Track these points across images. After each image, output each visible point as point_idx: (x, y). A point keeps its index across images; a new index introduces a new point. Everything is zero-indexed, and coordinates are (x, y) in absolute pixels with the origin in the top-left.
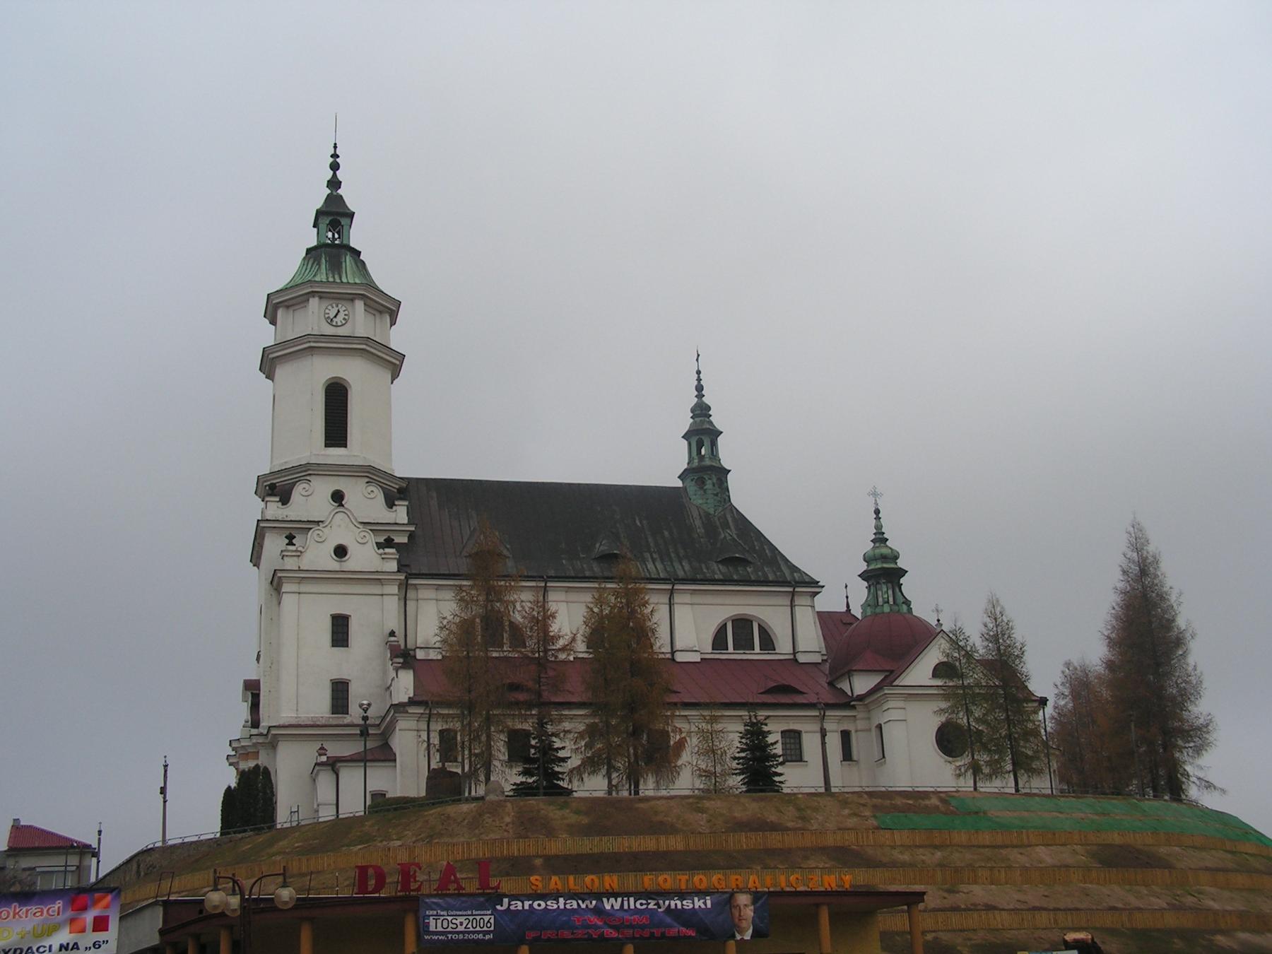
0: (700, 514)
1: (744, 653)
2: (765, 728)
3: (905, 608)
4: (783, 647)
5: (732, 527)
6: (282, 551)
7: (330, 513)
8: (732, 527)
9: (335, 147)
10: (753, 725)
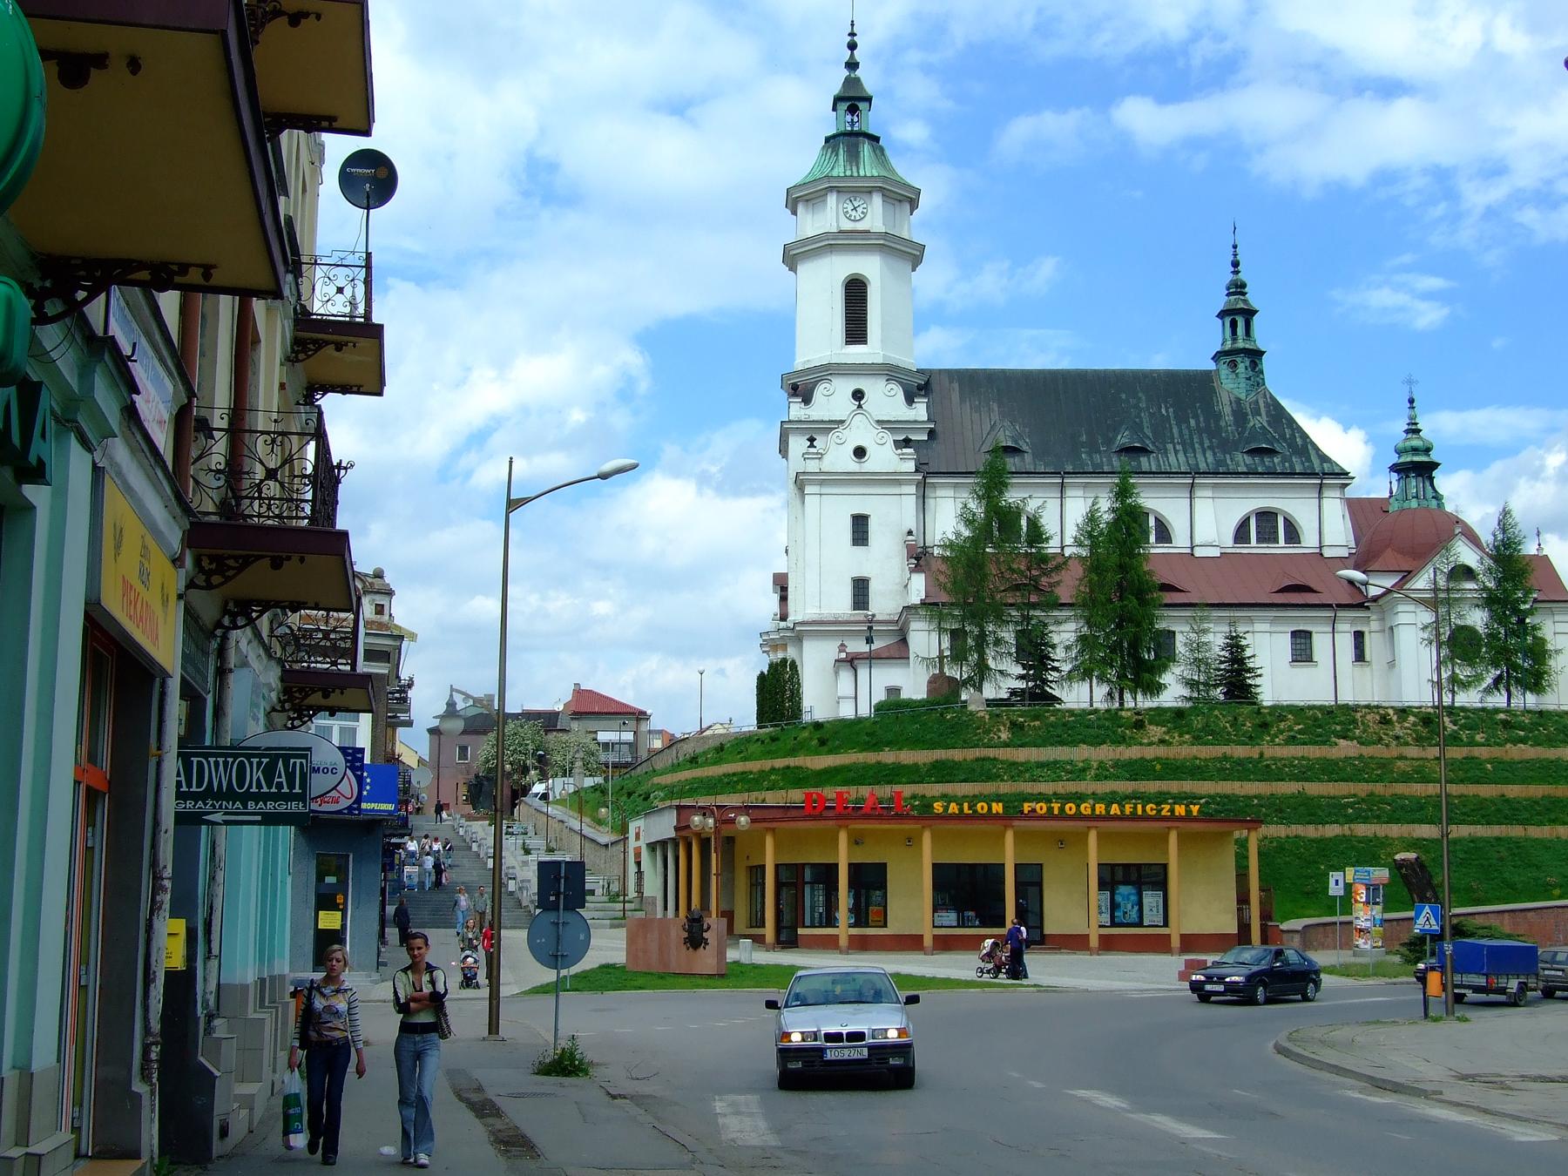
0: (1230, 401)
1: (1268, 547)
2: (1243, 642)
3: (1434, 502)
4: (1309, 540)
5: (1263, 413)
6: (803, 454)
7: (850, 414)
8: (1263, 413)
9: (852, 25)
10: (1232, 638)
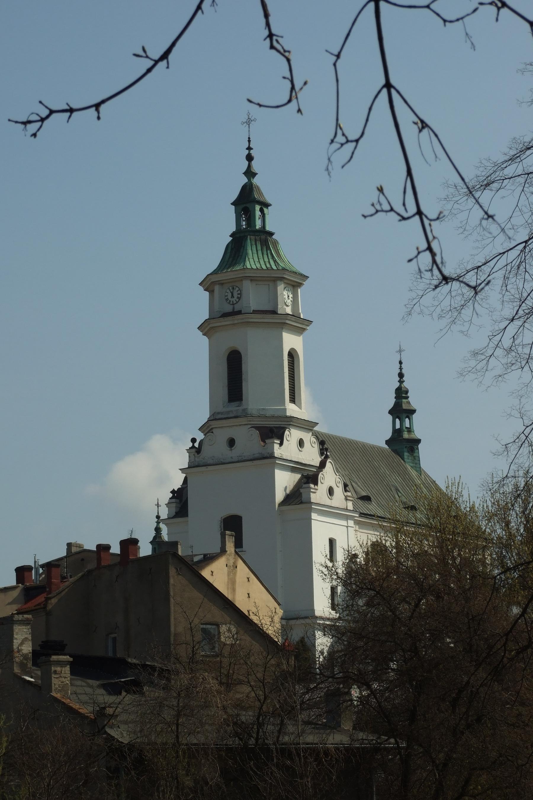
9: (249, 141)
